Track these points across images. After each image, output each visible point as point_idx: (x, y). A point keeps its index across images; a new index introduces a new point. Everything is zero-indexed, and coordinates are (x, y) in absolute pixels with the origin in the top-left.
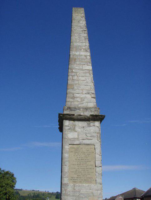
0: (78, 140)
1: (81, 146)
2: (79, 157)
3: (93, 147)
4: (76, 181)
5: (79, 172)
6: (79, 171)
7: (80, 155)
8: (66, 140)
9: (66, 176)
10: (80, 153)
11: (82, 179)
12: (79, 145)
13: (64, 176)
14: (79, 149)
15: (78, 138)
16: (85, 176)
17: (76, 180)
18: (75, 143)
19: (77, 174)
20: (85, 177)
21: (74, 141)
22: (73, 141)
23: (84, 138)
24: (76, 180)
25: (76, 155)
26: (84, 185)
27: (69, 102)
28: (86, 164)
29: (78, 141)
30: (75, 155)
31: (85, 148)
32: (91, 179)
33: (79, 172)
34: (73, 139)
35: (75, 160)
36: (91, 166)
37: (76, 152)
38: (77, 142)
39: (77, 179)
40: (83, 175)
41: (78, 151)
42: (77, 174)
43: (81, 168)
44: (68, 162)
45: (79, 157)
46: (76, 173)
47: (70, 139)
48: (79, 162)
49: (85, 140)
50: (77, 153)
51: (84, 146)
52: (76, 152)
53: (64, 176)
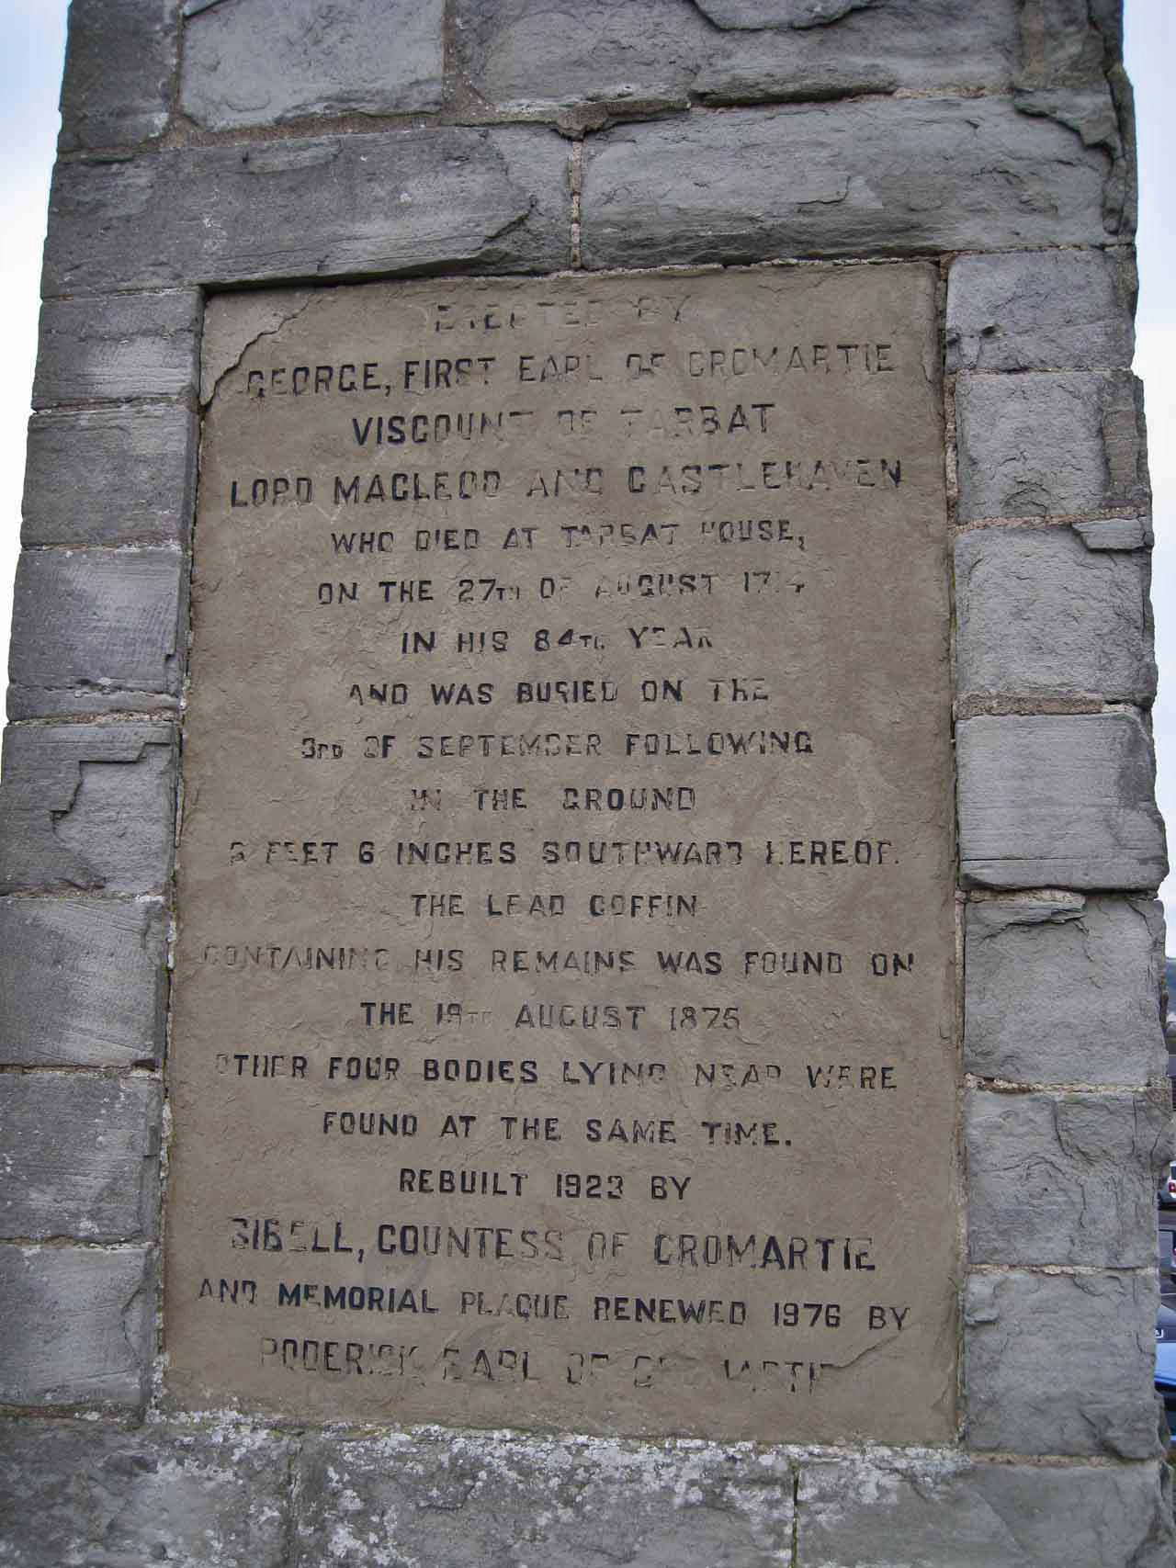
0: (458, 157)
1: (539, 318)
2: (484, 615)
3: (869, 299)
4: (371, 1325)
5: (473, 1071)
6: (452, 1043)
7: (486, 560)
8: (140, 176)
9: (93, 1181)
10: (489, 510)
11: (537, 1278)
12: (469, 298)
13: (40, 1200)
14: (476, 396)
15: (441, 111)
16: (637, 1189)
17: (371, 1298)
18: (372, 240)
19: (402, 1125)
20: (641, 1218)
21: (324, 197)
22: (301, 179)
23: (636, 90)
24: (371, 1298)
25: (398, 563)
26: (606, 1452)
27: (1050, 33)
28: (659, 825)
29: (449, 181)
30: (366, 572)
31: (644, 364)
32: (440, 514)
33: (473, 1071)
34: (324, 142)
35: (353, 725)
36: (813, 892)
37: (402, 489)
38: (431, 210)
39: (393, 1276)
40: (574, 1155)
41: (454, 452)
42: (402, 1125)
43: (523, 931)
44: (144, 784)
45: (484, 615)
46: (366, 1099)
47: (240, 159)
48: (452, 780)
49: (650, 138)
50: (403, 523)
51: (621, 296)
52: (402, 489)
53: (40, 1200)
